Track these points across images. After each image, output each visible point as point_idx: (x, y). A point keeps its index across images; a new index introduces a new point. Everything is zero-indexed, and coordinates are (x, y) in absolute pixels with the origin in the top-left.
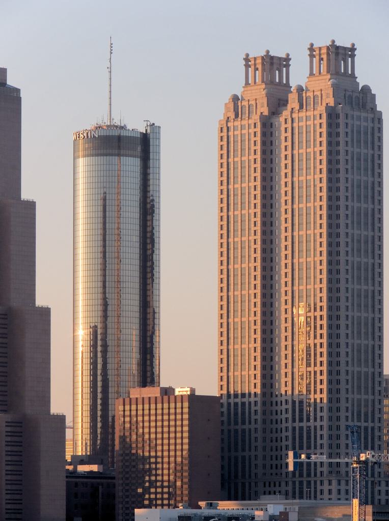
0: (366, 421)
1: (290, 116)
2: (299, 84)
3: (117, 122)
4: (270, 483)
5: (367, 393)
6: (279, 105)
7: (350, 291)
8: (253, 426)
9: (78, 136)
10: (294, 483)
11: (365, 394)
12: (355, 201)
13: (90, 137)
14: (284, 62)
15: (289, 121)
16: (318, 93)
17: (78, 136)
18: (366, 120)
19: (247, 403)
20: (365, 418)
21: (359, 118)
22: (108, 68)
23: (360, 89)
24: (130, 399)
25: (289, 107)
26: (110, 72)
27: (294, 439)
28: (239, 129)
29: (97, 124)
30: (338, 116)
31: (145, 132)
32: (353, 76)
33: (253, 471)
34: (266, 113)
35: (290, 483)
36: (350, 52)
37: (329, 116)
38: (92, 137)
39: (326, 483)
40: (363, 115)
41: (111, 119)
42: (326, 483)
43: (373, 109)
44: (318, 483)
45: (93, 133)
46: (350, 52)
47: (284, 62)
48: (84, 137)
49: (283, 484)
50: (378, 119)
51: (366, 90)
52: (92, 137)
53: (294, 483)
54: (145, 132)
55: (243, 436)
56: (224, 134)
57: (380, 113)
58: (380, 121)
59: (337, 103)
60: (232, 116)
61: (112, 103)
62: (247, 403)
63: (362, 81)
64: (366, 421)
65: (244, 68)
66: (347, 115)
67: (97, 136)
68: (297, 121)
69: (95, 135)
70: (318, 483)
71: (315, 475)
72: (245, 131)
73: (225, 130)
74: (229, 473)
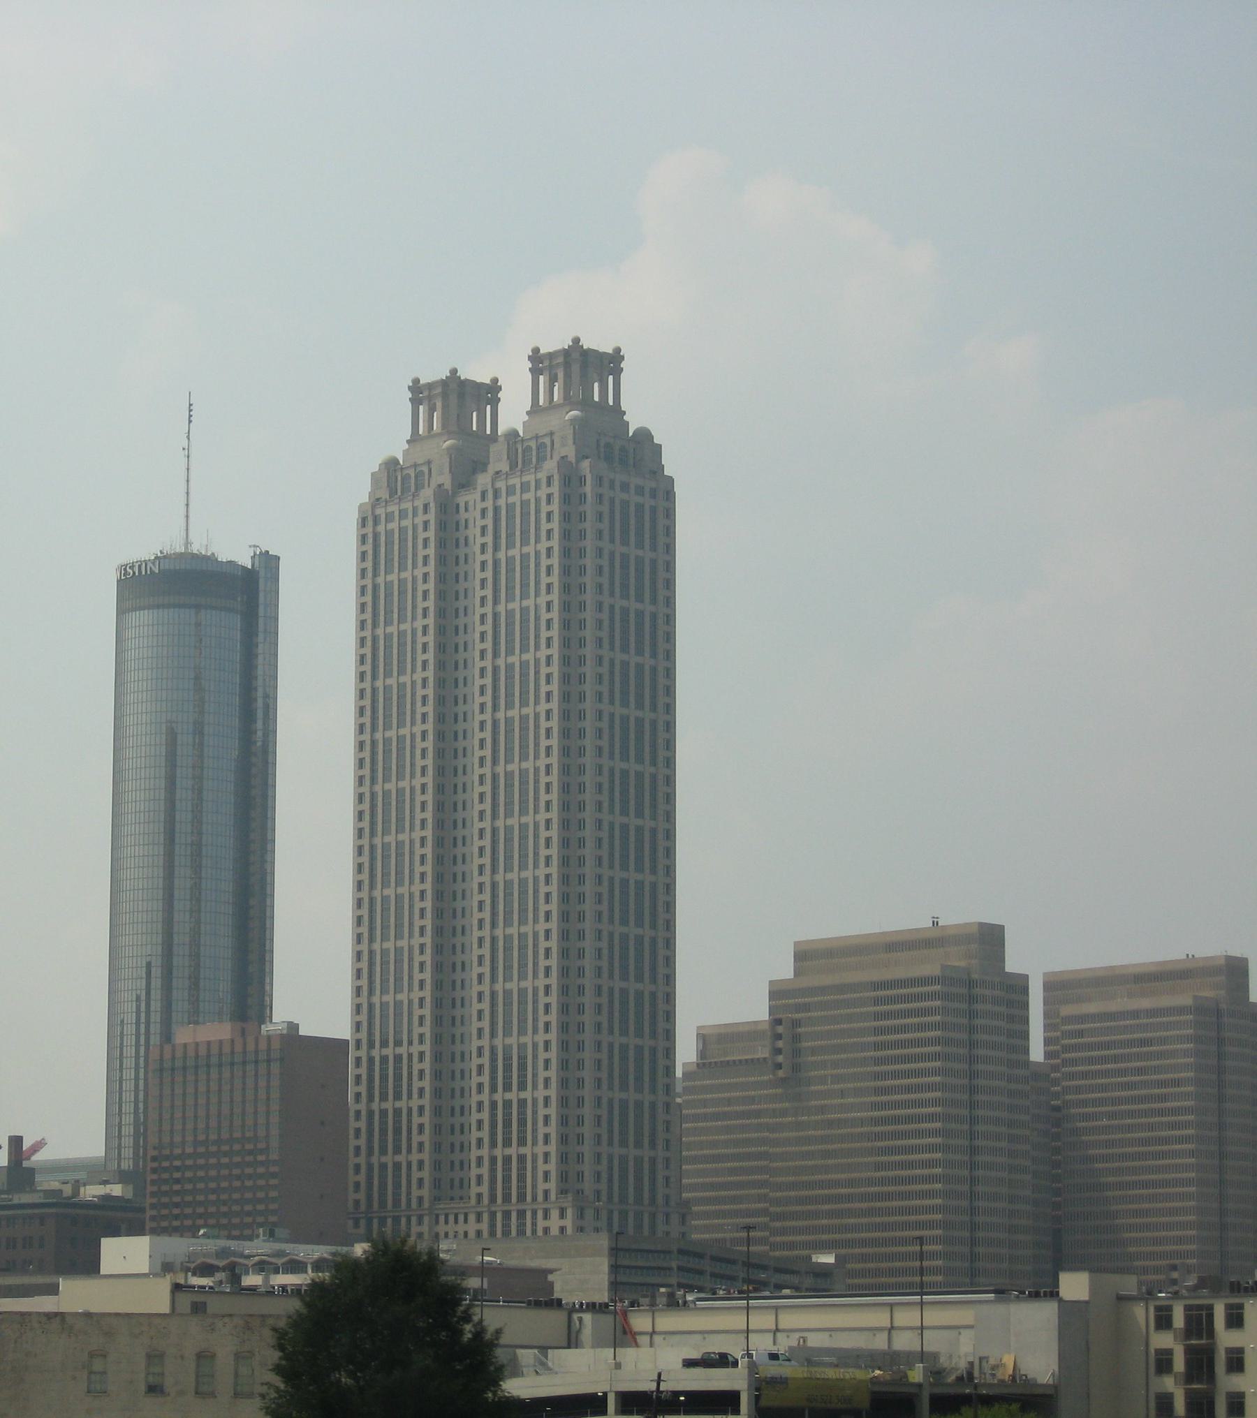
0: (625, 596)
1: (490, 486)
2: (515, 427)
3: (196, 548)
4: (447, 1216)
5: (639, 923)
6: (474, 472)
7: (606, 826)
8: (415, 1103)
9: (123, 572)
10: (493, 1215)
11: (622, 760)
12: (617, 703)
13: (144, 573)
14: (489, 393)
15: (490, 495)
16: (547, 441)
17: (123, 572)
18: (640, 490)
19: (405, 1057)
20: (380, 1147)
21: (625, 487)
22: (184, 449)
23: (631, 434)
24: (174, 1046)
25: (492, 469)
26: (188, 457)
27: (493, 1125)
28: (397, 518)
29: (161, 552)
30: (582, 481)
31: (250, 567)
32: (618, 411)
33: (415, 1193)
34: (448, 485)
35: (486, 1217)
36: (611, 363)
37: (566, 481)
38: (149, 572)
39: (555, 1214)
40: (635, 481)
41: (187, 543)
42: (555, 1214)
43: (657, 470)
44: (540, 1214)
45: (150, 565)
46: (611, 363)
47: (489, 393)
48: (134, 573)
49: (472, 1218)
50: (665, 492)
51: (644, 436)
52: (149, 572)
53: (493, 1215)
54: (250, 567)
55: (397, 1122)
56: (369, 530)
57: (671, 480)
58: (670, 495)
59: (581, 457)
60: (384, 494)
61: (191, 515)
62: (405, 1057)
63: (635, 420)
64: (639, 1089)
65: (409, 406)
66: (601, 479)
67: (157, 571)
68: (504, 494)
69: (153, 567)
70: (540, 1214)
71: (534, 1199)
72: (407, 523)
73: (370, 523)
74: (369, 1198)
